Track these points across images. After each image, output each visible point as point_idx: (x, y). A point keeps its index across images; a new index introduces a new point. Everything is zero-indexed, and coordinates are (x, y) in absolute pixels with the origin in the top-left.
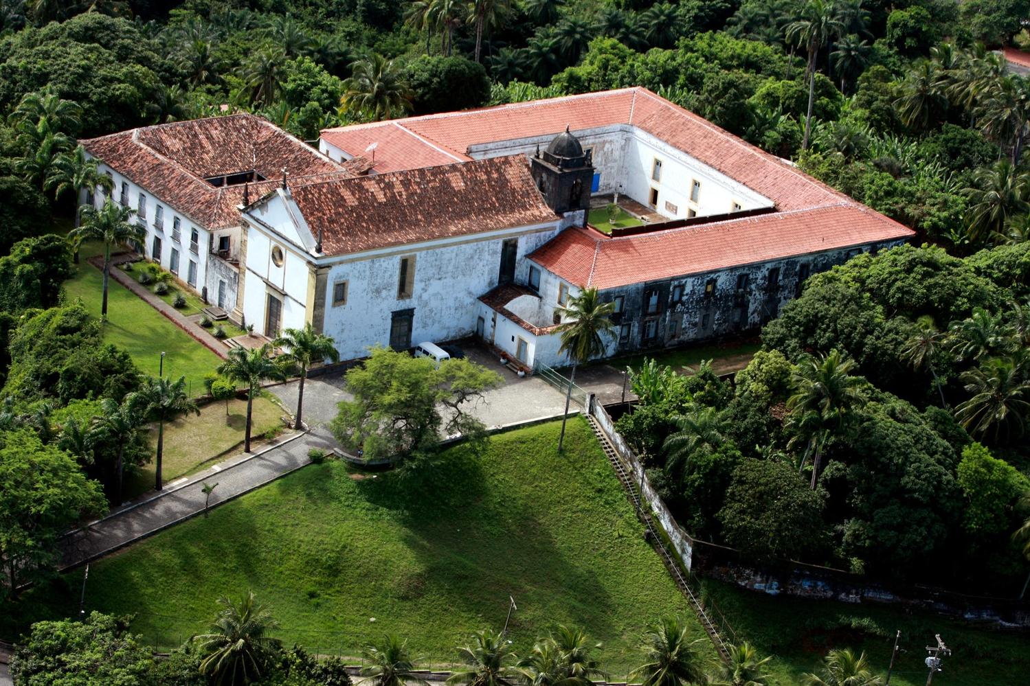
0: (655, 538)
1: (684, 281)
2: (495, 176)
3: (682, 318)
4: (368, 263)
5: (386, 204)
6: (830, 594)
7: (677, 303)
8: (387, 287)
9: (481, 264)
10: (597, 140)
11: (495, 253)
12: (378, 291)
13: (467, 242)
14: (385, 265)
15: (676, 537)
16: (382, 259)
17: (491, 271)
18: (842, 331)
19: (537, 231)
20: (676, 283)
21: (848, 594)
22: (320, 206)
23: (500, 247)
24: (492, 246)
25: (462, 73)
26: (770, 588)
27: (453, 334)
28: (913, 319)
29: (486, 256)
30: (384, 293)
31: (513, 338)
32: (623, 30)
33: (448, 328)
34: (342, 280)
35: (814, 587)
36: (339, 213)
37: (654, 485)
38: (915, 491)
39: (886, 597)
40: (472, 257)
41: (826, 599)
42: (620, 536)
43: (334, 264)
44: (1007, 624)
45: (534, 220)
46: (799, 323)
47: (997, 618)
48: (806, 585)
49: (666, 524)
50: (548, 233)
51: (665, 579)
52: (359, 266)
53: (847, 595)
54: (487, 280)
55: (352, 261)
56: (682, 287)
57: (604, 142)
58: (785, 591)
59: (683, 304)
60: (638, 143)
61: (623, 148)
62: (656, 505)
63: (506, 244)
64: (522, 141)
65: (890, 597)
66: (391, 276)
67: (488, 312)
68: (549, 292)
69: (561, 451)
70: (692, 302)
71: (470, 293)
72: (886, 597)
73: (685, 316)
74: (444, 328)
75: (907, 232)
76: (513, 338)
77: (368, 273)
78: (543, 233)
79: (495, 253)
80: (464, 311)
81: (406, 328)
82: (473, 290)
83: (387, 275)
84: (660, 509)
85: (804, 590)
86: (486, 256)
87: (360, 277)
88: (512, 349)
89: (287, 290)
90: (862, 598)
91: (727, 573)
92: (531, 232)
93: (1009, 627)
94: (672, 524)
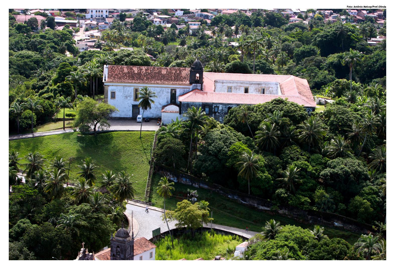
1: (218, 105)
2: (178, 72)
3: (219, 118)
4: (122, 87)
5: (136, 74)
6: (191, 184)
7: (217, 112)
8: (130, 96)
9: (163, 95)
10: (266, 86)
11: (168, 92)
12: (126, 97)
13: (157, 87)
14: (128, 89)
16: (127, 87)
17: (167, 98)
19: (183, 88)
20: (215, 105)
21: (195, 184)
22: (115, 71)
23: (170, 91)
24: (168, 90)
25: (237, 65)
26: (175, 180)
27: (155, 116)
29: (165, 93)
30: (129, 98)
33: (153, 114)
34: (113, 91)
35: (186, 181)
36: (120, 74)
38: (211, 151)
39: (206, 187)
40: (160, 92)
41: (190, 185)
42: (142, 161)
43: (110, 85)
44: (244, 202)
45: (185, 85)
47: (240, 199)
48: (184, 180)
50: (188, 89)
52: (119, 87)
53: (195, 185)
54: (166, 101)
55: (117, 86)
56: (218, 107)
57: (269, 87)
58: (179, 181)
59: (219, 113)
63: (172, 90)
64: (237, 81)
65: (207, 187)
66: (131, 93)
69: (140, 138)
70: (222, 113)
71: (160, 104)
72: (206, 187)
73: (220, 117)
74: (151, 113)
77: (122, 90)
78: (185, 89)
79: (168, 92)
80: (158, 109)
81: (138, 111)
82: (160, 103)
83: (129, 92)
85: (184, 181)
86: (165, 93)
87: (120, 91)
90: (199, 186)
91: (163, 173)
92: (181, 88)
93: (244, 203)
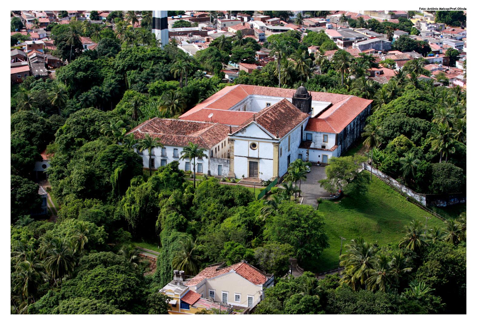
0: (410, 200)
15: (417, 197)
18: (412, 125)
28: (58, 304)
31: (319, 156)
32: (103, 93)
37: (402, 184)
46: (397, 127)
49: (410, 194)
51: (421, 210)
60: (257, 100)
61: (251, 104)
62: (404, 189)
67: (304, 151)
68: (318, 140)
75: (272, 139)
76: (319, 156)
84: (406, 190)
88: (320, 159)
89: (260, 157)
94: (413, 193)
